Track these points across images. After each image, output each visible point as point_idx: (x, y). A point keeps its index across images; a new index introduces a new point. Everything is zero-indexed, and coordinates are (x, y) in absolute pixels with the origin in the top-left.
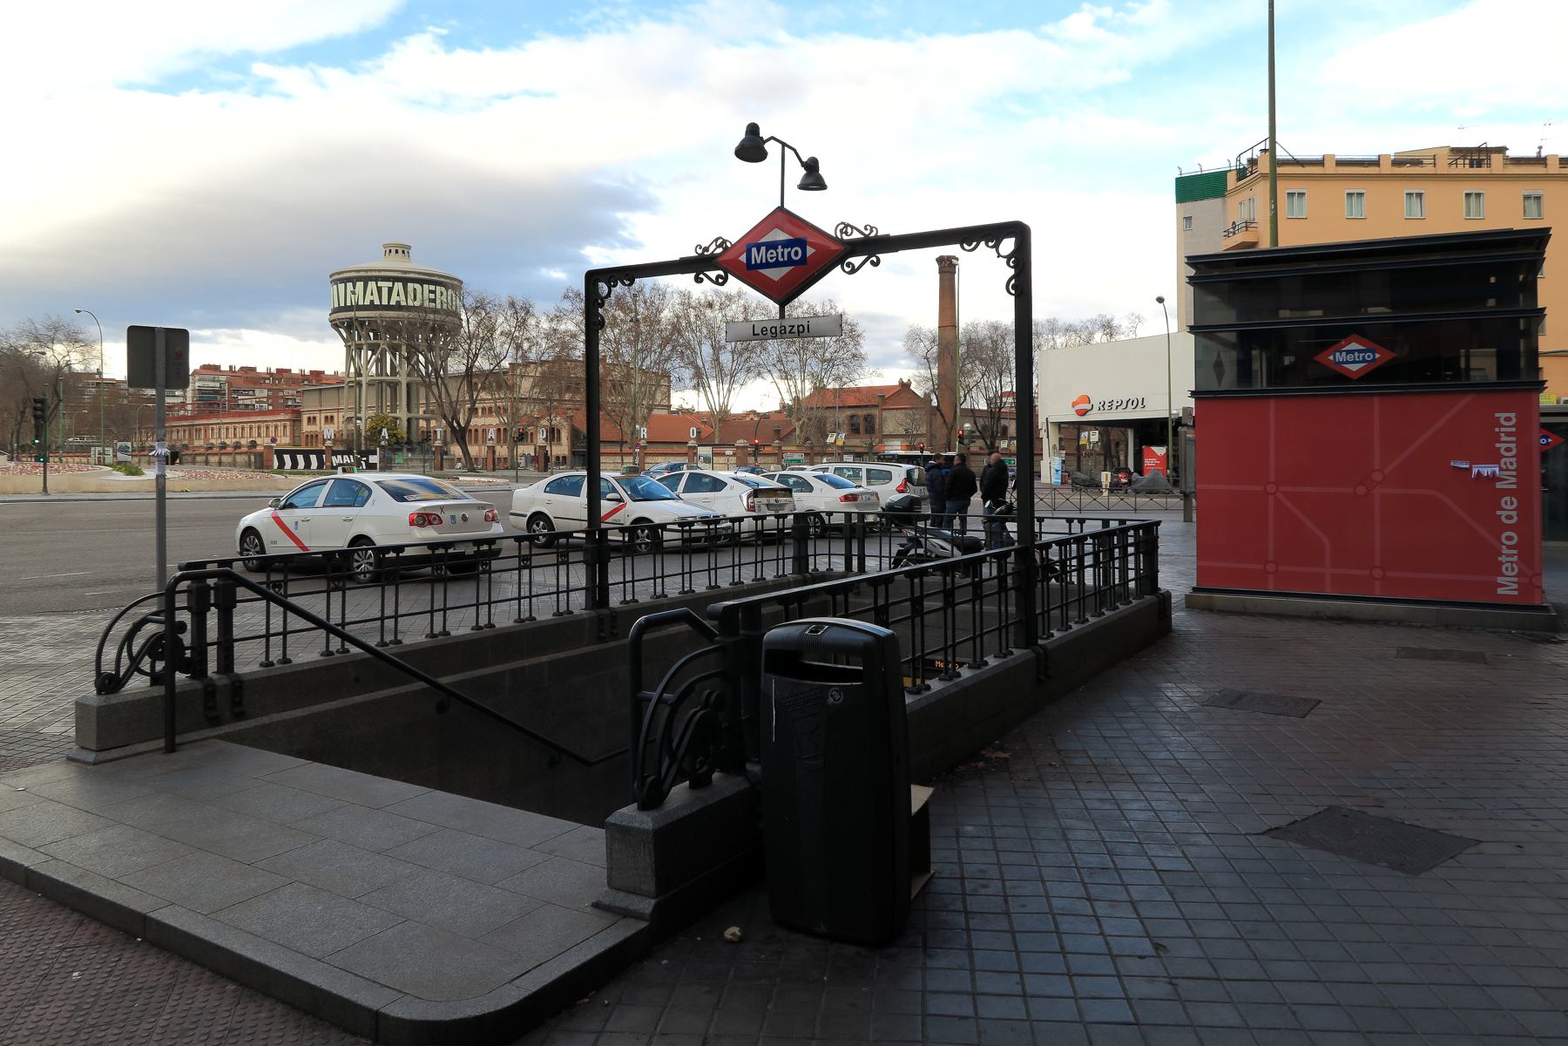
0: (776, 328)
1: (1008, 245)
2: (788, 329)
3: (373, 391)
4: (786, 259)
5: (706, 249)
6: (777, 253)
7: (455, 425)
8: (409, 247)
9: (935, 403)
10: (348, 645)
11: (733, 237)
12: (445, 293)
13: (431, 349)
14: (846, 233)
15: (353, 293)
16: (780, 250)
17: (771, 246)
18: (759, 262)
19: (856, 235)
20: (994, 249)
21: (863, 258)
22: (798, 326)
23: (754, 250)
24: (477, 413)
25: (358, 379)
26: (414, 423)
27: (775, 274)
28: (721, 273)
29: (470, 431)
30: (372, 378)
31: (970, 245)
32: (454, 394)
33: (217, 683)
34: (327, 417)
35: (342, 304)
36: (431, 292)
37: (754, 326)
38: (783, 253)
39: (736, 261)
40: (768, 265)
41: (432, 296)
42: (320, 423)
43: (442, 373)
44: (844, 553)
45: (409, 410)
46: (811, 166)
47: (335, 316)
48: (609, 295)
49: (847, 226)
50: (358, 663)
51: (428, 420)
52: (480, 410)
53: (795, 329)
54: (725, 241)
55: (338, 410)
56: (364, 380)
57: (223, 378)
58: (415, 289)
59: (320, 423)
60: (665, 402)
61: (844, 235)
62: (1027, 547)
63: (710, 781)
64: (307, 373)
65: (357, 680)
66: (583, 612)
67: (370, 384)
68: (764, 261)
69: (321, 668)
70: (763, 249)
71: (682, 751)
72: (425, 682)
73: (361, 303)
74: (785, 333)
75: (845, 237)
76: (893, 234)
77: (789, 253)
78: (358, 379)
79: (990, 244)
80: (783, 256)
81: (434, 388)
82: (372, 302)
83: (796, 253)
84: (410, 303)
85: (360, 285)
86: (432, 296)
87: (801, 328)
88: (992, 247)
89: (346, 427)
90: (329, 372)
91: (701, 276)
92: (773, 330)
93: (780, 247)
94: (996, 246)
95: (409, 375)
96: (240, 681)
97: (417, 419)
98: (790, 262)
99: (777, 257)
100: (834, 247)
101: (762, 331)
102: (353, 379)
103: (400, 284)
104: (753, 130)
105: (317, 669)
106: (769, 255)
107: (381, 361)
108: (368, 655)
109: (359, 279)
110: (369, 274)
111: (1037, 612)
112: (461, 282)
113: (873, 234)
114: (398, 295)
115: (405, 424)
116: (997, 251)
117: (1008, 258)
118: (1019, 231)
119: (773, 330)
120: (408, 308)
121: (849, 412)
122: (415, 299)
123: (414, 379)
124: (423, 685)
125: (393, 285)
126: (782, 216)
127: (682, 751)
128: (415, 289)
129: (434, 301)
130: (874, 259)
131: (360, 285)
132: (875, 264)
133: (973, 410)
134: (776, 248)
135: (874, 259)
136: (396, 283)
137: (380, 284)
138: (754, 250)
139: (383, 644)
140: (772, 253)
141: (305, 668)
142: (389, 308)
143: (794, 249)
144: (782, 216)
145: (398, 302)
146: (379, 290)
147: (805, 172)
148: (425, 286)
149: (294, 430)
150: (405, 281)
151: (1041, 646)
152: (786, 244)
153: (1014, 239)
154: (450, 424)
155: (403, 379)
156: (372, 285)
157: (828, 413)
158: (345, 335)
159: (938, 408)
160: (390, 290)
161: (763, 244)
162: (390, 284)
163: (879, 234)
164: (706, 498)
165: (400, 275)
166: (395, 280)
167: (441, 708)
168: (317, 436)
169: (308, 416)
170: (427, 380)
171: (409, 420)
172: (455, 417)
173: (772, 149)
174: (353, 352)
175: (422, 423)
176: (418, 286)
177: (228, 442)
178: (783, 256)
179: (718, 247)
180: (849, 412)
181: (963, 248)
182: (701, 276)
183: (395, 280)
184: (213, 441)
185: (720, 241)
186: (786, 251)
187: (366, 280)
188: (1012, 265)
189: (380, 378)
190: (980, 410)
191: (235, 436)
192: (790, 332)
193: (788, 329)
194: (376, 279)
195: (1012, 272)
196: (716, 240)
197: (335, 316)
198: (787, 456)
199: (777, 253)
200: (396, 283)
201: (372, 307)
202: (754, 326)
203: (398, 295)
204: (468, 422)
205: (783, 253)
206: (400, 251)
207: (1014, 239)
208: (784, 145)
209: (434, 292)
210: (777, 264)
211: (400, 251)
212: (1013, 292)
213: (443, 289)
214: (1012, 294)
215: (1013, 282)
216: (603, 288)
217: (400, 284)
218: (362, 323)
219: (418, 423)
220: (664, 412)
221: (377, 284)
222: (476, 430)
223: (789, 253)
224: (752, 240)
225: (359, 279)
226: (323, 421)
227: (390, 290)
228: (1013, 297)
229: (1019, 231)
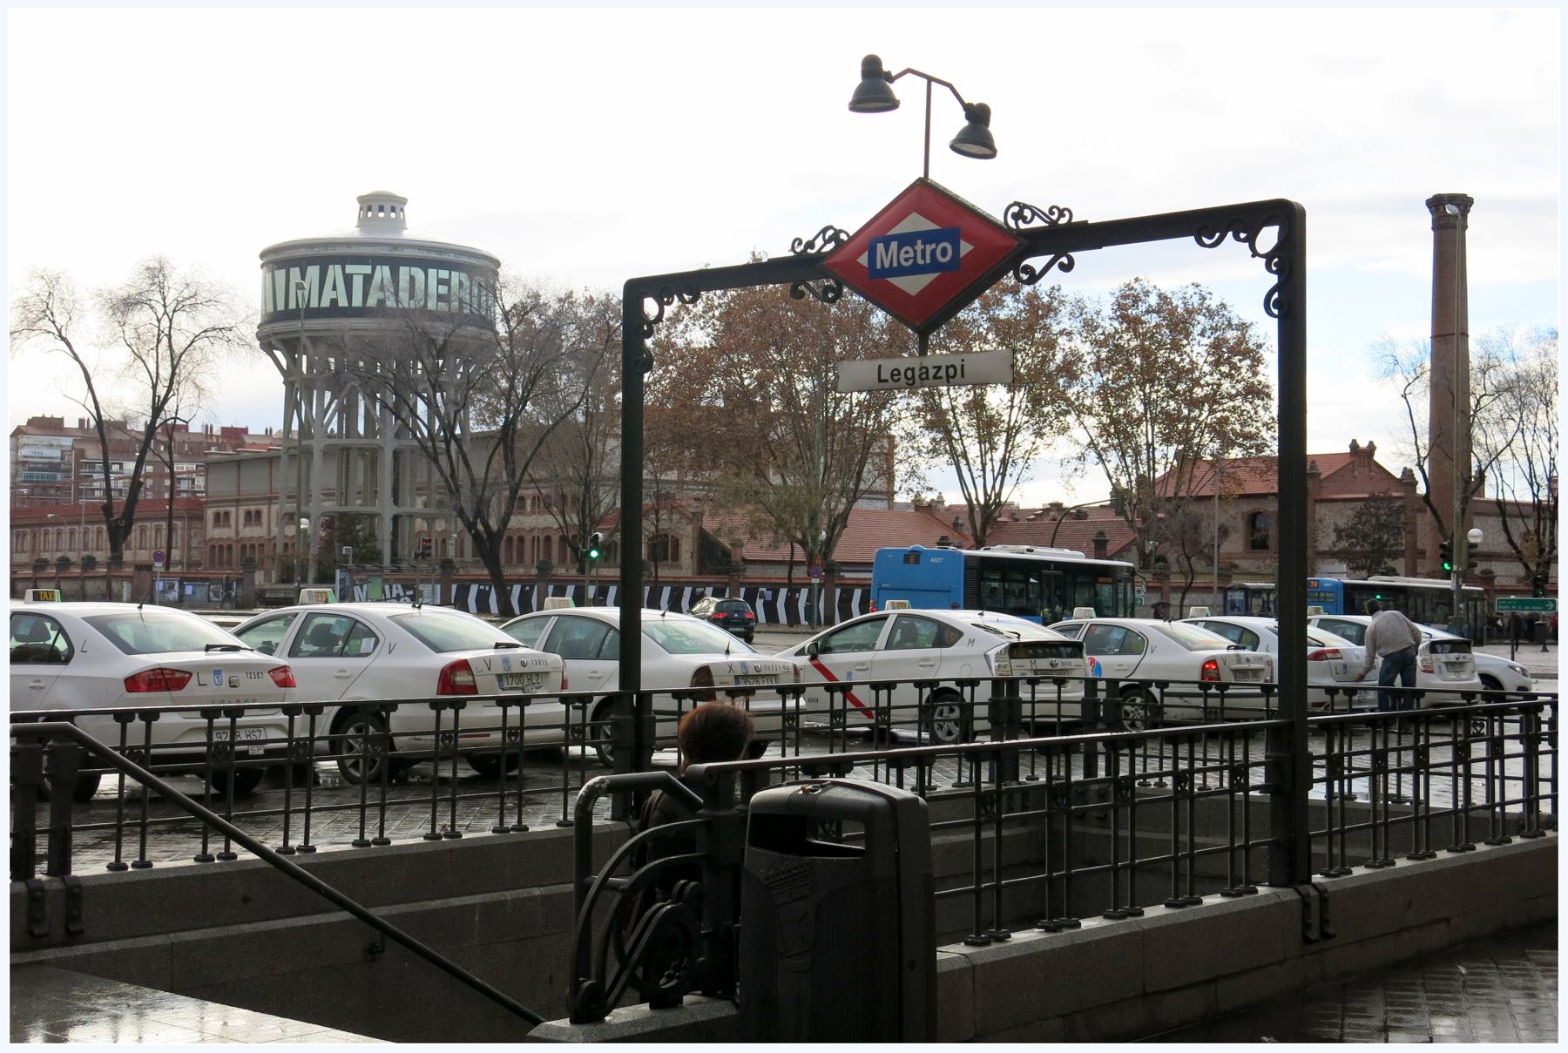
0: (913, 370)
1: (1269, 237)
2: (932, 372)
3: (333, 468)
4: (928, 261)
5: (811, 244)
6: (915, 252)
7: (480, 527)
8: (403, 201)
9: (1421, 489)
10: (235, 847)
11: (851, 223)
12: (467, 283)
13: (436, 386)
14: (1025, 220)
15: (300, 287)
16: (919, 246)
17: (906, 240)
18: (887, 265)
19: (1038, 223)
20: (1247, 244)
21: (1049, 257)
22: (947, 367)
23: (880, 247)
24: (523, 507)
25: (304, 443)
26: (405, 525)
27: (913, 285)
28: (832, 282)
29: (510, 539)
30: (332, 441)
31: (1210, 237)
32: (479, 472)
33: (46, 887)
34: (248, 513)
35: (281, 307)
36: (440, 282)
37: (880, 366)
38: (923, 252)
39: (852, 263)
40: (901, 271)
41: (443, 290)
42: (237, 523)
43: (458, 431)
45: (396, 502)
46: (978, 116)
47: (279, 326)
48: (659, 318)
49: (1023, 207)
50: (247, 871)
51: (430, 519)
52: (529, 502)
53: (942, 373)
54: (838, 232)
55: (270, 500)
56: (317, 445)
57: (67, 442)
58: (412, 279)
59: (237, 523)
60: (880, 484)
61: (1020, 222)
62: (1292, 722)
63: (681, 1001)
64: (217, 431)
65: (246, 900)
66: (609, 822)
67: (327, 452)
68: (895, 265)
69: (194, 877)
70: (894, 245)
71: (636, 955)
72: (351, 912)
73: (314, 304)
74: (927, 378)
75: (1022, 226)
76: (1091, 221)
77: (933, 252)
78: (304, 443)
79: (1243, 235)
80: (923, 257)
81: (443, 459)
82: (334, 302)
83: (943, 252)
85: (313, 271)
86: (443, 290)
87: (951, 371)
88: (1244, 240)
89: (281, 530)
90: (256, 429)
91: (802, 288)
92: (909, 374)
93: (919, 242)
94: (1251, 240)
95: (397, 436)
96: (79, 887)
97: (411, 516)
98: (934, 266)
99: (915, 258)
100: (1004, 242)
101: (892, 375)
102: (296, 444)
103: (386, 269)
104: (872, 68)
105: (187, 878)
106: (902, 256)
107: (348, 412)
108: (265, 864)
109: (312, 261)
110: (331, 251)
112: (498, 264)
113: (1063, 221)
114: (334, 288)
115: (387, 527)
116: (1253, 248)
117: (1269, 257)
118: (1287, 216)
119: (909, 374)
121: (1247, 507)
122: (412, 296)
123: (407, 442)
124: (346, 915)
125: (373, 270)
126: (925, 195)
127: (636, 955)
128: (412, 279)
130: (1064, 260)
131: (313, 271)
132: (1067, 268)
133: (1500, 504)
134: (913, 245)
135: (1064, 260)
136: (378, 267)
137: (350, 269)
138: (880, 247)
139: (287, 850)
140: (907, 252)
141: (171, 875)
143: (942, 245)
144: (925, 195)
146: (348, 280)
147: (966, 123)
148: (431, 272)
149: (189, 536)
151: (1315, 886)
152: (927, 237)
153: (1276, 228)
154: (470, 526)
155: (389, 445)
156: (335, 271)
158: (284, 362)
159: (1426, 498)
160: (368, 279)
161: (894, 238)
162: (367, 269)
163: (1074, 220)
164: (925, 659)
165: (386, 252)
166: (375, 261)
167: (372, 952)
168: (230, 547)
169: (246, 508)
170: (430, 444)
171: (396, 519)
172: (480, 513)
173: (906, 90)
174: (297, 388)
175: (420, 524)
176: (418, 273)
177: (73, 556)
178: (923, 257)
179: (826, 242)
180: (1247, 507)
181: (1202, 244)
182: (802, 288)
183: (375, 261)
184: (45, 556)
185: (830, 232)
186: (929, 248)
187: (324, 262)
188: (1274, 268)
190: (1517, 504)
191: (86, 548)
192: (935, 377)
193: (932, 372)
194: (343, 260)
195: (1273, 280)
196: (824, 231)
197: (279, 326)
199: (915, 252)
200: (378, 267)
201: (334, 310)
202: (880, 366)
203: (334, 288)
204: (504, 522)
205: (923, 252)
207: (1276, 228)
208: (930, 79)
209: (446, 282)
210: (915, 270)
212: (1276, 312)
213: (464, 277)
214: (1271, 314)
215: (1276, 296)
216: (650, 306)
217: (386, 269)
218: (315, 340)
219: (412, 525)
220: (881, 505)
221: (343, 270)
222: (521, 539)
223: (933, 252)
224: (880, 229)
225: (312, 261)
226: (242, 520)
227: (368, 279)
228: (1276, 320)
229: (1287, 216)
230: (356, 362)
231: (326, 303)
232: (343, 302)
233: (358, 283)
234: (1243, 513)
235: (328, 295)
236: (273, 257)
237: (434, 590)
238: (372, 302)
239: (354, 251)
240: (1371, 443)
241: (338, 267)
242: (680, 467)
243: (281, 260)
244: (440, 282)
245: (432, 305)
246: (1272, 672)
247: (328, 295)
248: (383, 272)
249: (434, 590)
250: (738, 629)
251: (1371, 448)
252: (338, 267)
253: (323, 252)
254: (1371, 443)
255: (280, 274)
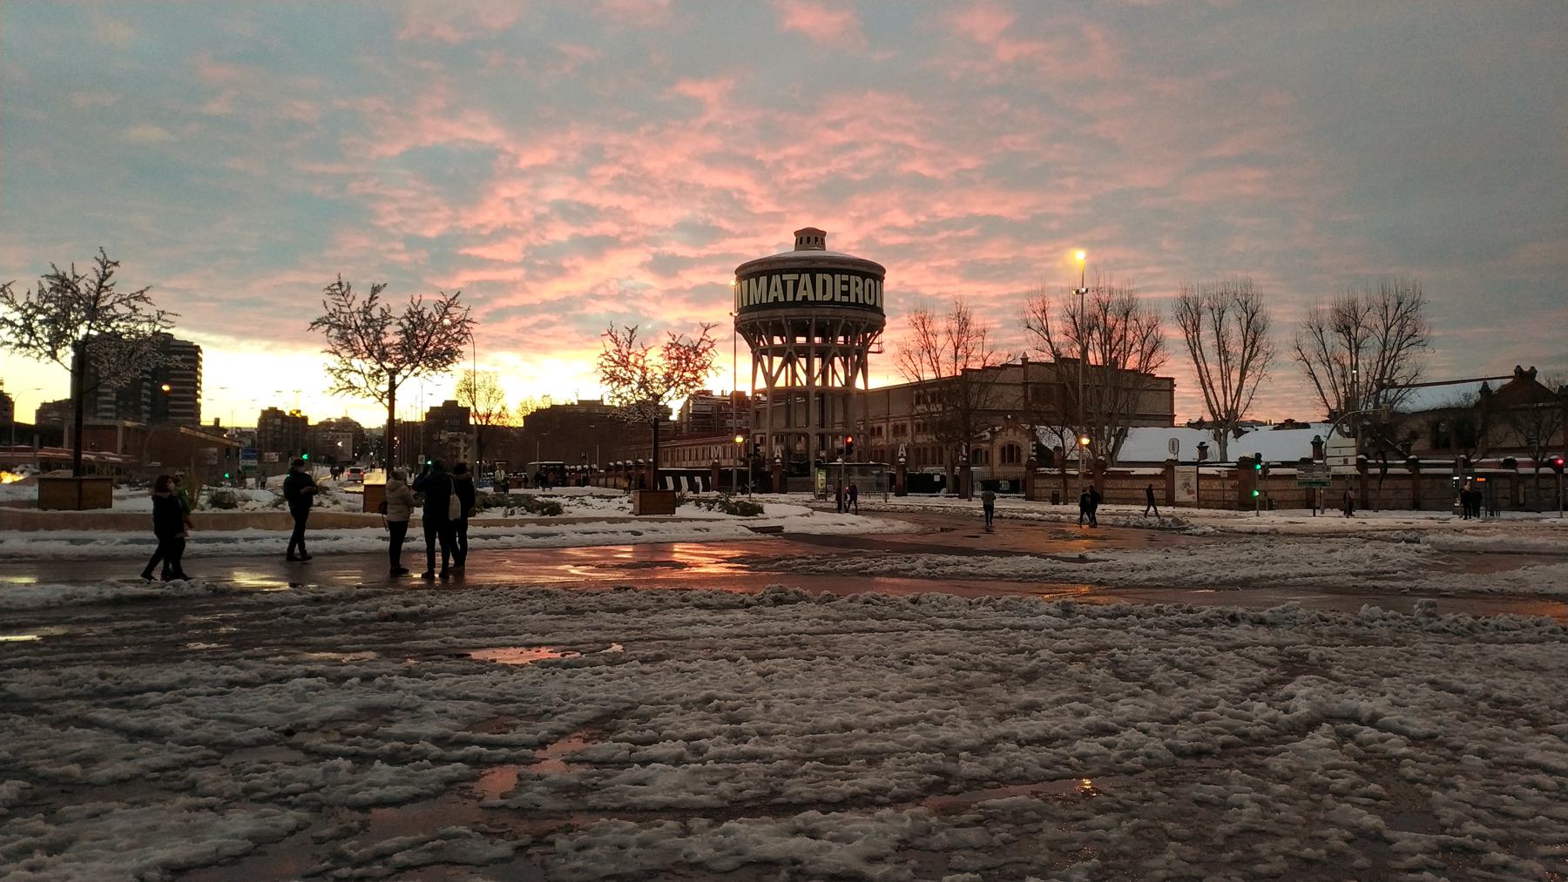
12: (861, 283)
35: (745, 305)
36: (843, 283)
41: (845, 288)
44: (870, 387)
58: (824, 281)
73: (764, 301)
82: (805, 298)
84: (819, 297)
85: (763, 280)
86: (845, 288)
109: (775, 272)
111: (780, 343)
114: (805, 289)
120: (815, 303)
122: (824, 293)
125: (800, 277)
128: (824, 281)
129: (847, 293)
131: (763, 280)
137: (785, 277)
142: (795, 304)
145: (805, 298)
148: (853, 300)
150: (813, 273)
156: (776, 279)
157: (1317, 487)
160: (796, 283)
162: (795, 277)
176: (828, 277)
183: (801, 271)
189: (788, 430)
194: (781, 272)
198: (1170, 520)
203: (805, 289)
206: (813, 240)
211: (813, 240)
213: (859, 279)
225: (762, 274)
227: (796, 283)
230: (825, 340)
231: (771, 300)
232: (781, 299)
233: (790, 285)
234: (1429, 422)
235: (773, 294)
236: (742, 272)
237: (311, 539)
238: (799, 298)
239: (787, 265)
240: (1533, 368)
241: (778, 276)
242: (925, 402)
243: (750, 272)
244: (843, 283)
245: (837, 299)
246: (1531, 519)
247: (773, 294)
248: (806, 278)
249: (311, 539)
250: (728, 553)
251: (1533, 372)
252: (778, 276)
253: (769, 268)
254: (1533, 368)
255: (745, 283)
